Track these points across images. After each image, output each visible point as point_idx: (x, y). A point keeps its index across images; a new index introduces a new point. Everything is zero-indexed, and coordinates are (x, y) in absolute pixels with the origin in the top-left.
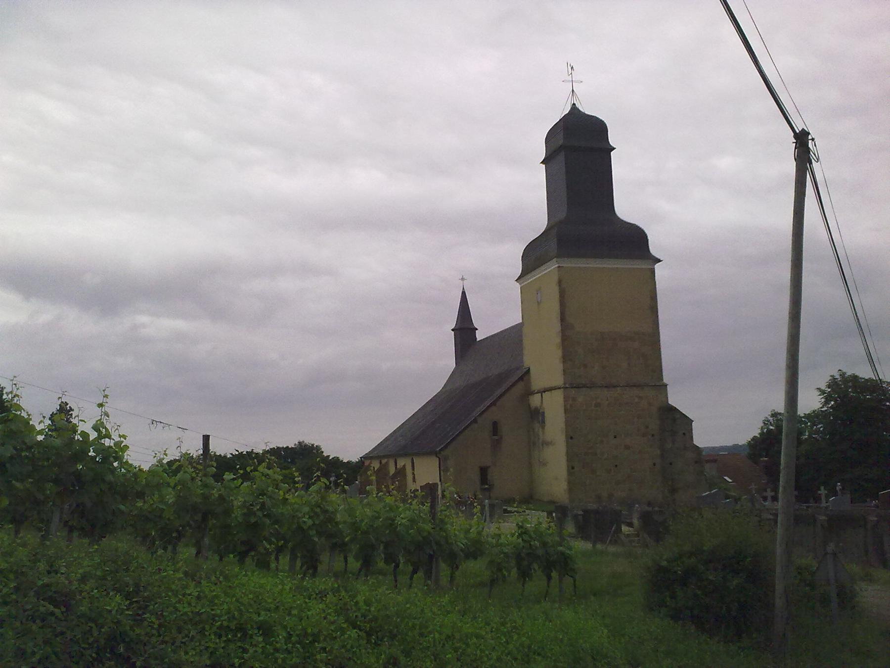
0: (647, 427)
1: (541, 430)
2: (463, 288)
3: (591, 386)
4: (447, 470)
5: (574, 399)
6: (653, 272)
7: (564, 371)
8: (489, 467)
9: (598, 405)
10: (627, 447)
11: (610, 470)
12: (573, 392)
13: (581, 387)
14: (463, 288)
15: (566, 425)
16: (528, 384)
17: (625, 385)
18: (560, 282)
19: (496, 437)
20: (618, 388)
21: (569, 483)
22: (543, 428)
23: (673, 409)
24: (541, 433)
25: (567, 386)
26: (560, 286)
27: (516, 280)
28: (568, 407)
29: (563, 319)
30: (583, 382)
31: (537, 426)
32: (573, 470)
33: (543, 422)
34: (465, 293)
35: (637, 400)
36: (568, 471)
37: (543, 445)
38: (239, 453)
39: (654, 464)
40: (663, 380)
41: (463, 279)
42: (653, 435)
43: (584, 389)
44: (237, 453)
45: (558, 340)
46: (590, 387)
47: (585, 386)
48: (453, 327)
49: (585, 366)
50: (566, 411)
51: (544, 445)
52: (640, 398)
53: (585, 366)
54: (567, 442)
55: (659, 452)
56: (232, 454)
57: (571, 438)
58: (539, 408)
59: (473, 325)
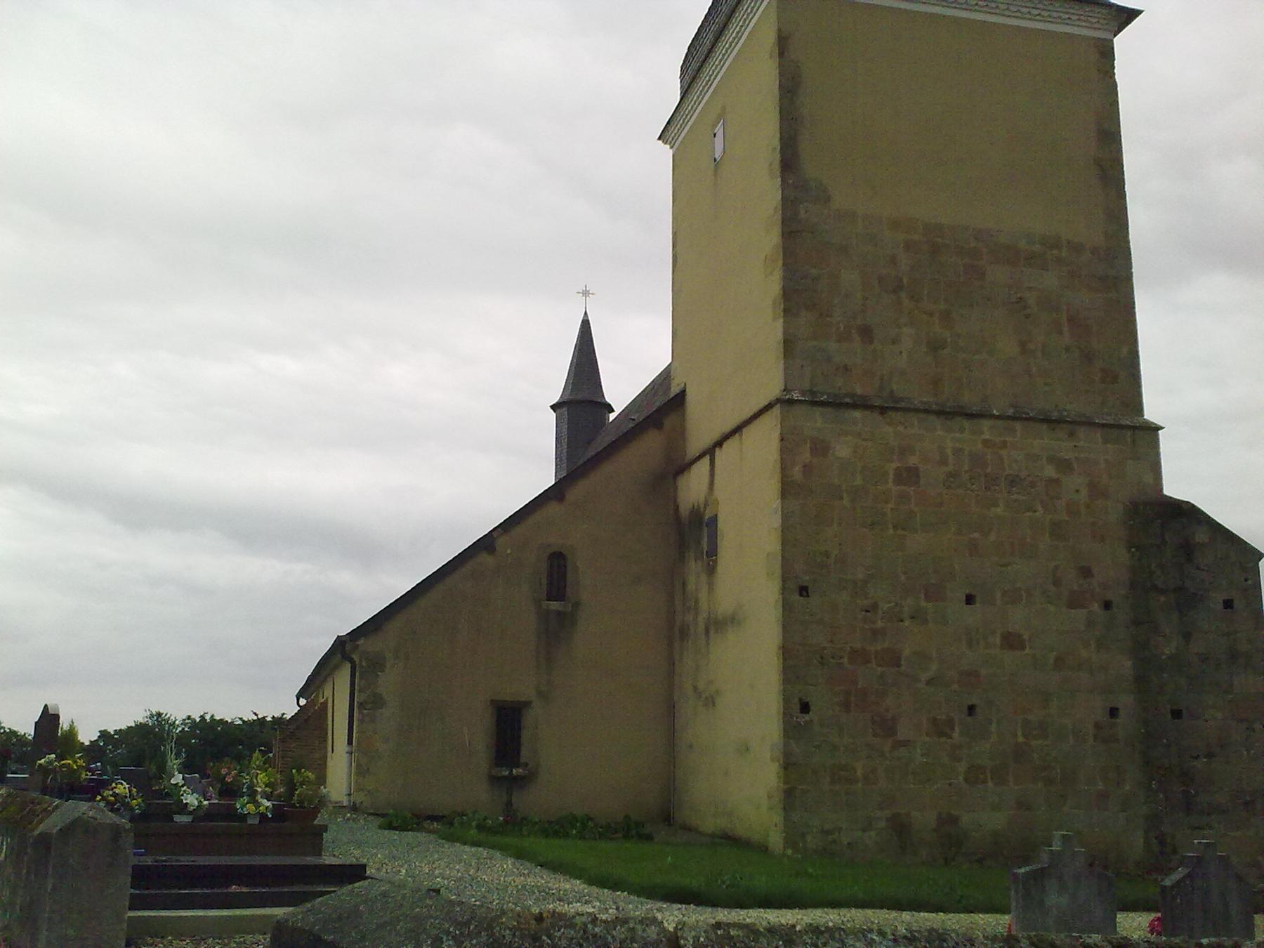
0: (1086, 572)
1: (704, 578)
2: (586, 313)
3: (887, 407)
4: (377, 702)
5: (820, 448)
6: (1107, 54)
7: (789, 346)
8: (527, 704)
9: (909, 476)
10: (1012, 641)
11: (950, 723)
12: (815, 422)
13: (847, 406)
14: (586, 313)
15: (784, 543)
16: (681, 433)
17: (1011, 412)
18: (783, 43)
19: (554, 605)
20: (986, 424)
21: (788, 765)
22: (711, 570)
23: (1186, 513)
24: (703, 595)
25: (796, 396)
26: (781, 54)
27: (659, 138)
28: (797, 472)
29: (789, 162)
30: (859, 391)
31: (694, 568)
32: (807, 717)
33: (713, 552)
34: (589, 324)
35: (1050, 471)
36: (786, 714)
37: (707, 631)
38: (258, 718)
39: (1113, 712)
40: (1143, 416)
41: (586, 293)
42: (1107, 605)
43: (857, 414)
44: (255, 718)
45: (772, 239)
46: (883, 410)
47: (862, 404)
48: (555, 399)
49: (866, 333)
50: (787, 489)
51: (712, 632)
52: (1064, 466)
53: (866, 333)
54: (787, 607)
55: (1126, 665)
56: (241, 719)
57: (803, 591)
58: (702, 506)
59: (604, 398)
